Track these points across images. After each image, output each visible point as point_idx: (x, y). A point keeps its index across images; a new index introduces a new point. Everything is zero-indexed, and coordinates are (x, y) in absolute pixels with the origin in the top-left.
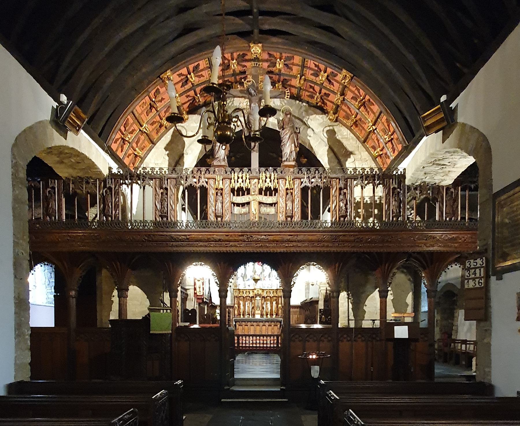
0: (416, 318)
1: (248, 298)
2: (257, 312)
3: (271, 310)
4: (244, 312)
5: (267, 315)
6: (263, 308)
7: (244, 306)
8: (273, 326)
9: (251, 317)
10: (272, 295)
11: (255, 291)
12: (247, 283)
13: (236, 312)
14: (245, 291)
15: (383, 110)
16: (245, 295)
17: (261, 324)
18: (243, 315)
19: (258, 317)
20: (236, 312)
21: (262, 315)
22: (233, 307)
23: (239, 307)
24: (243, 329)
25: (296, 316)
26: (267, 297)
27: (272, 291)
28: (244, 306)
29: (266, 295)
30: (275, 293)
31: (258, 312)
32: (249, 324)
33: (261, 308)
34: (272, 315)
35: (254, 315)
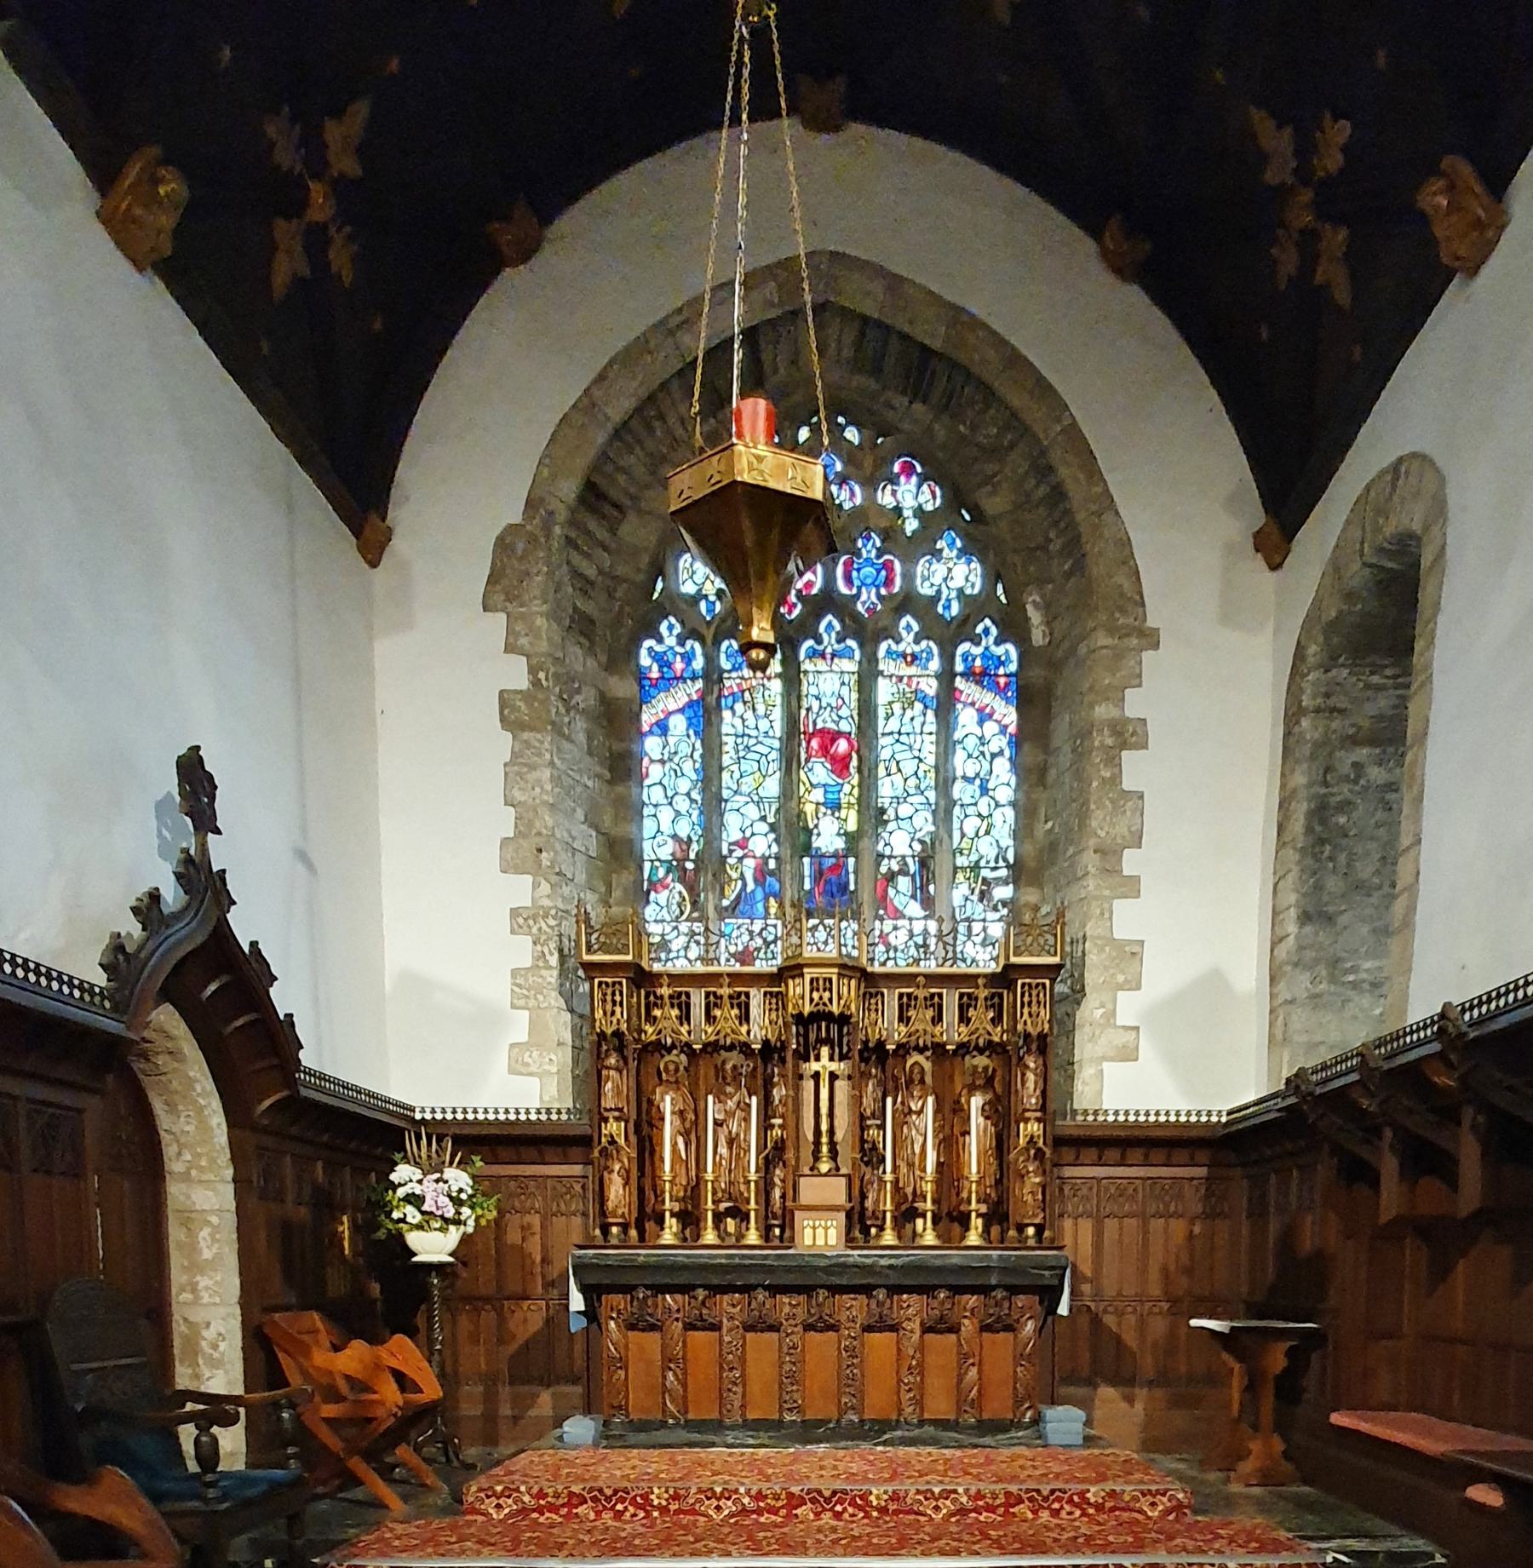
0: (1023, 1075)
1: (733, 1059)
2: (812, 1190)
3: (949, 1170)
4: (694, 1191)
5: (906, 1215)
6: (870, 1155)
7: (692, 1129)
8: (968, 1326)
9: (753, 1237)
10: (952, 1032)
11: (796, 989)
12: (738, 934)
13: (617, 1192)
14: (698, 998)
15: (1007, 753)
16: (699, 1031)
17: (853, 1308)
18: (690, 1219)
19: (821, 1235)
20: (617, 1192)
21: (859, 1222)
22: (585, 1142)
23: (647, 1147)
24: (668, 1360)
25: (1178, 1227)
26: (903, 1049)
27: (951, 1000)
28: (692, 1129)
29: (899, 1033)
30: (981, 1016)
31: (824, 1189)
32: (729, 1307)
33: (847, 1154)
34: (952, 1219)
35: (787, 1221)
